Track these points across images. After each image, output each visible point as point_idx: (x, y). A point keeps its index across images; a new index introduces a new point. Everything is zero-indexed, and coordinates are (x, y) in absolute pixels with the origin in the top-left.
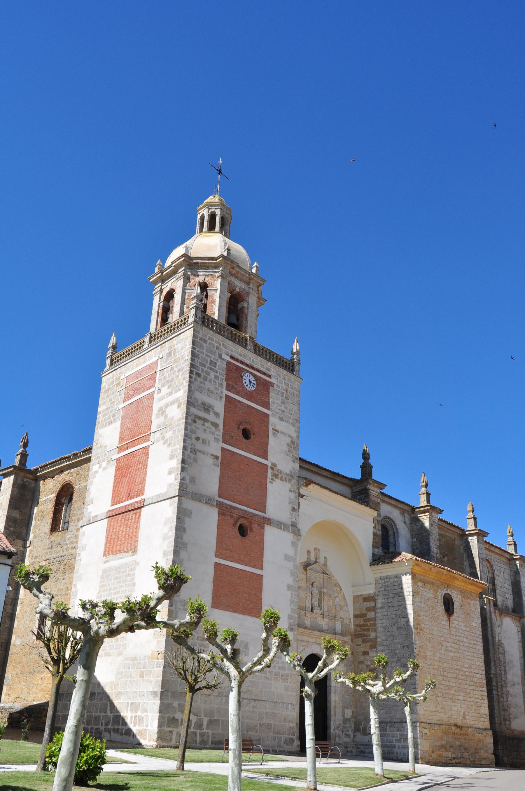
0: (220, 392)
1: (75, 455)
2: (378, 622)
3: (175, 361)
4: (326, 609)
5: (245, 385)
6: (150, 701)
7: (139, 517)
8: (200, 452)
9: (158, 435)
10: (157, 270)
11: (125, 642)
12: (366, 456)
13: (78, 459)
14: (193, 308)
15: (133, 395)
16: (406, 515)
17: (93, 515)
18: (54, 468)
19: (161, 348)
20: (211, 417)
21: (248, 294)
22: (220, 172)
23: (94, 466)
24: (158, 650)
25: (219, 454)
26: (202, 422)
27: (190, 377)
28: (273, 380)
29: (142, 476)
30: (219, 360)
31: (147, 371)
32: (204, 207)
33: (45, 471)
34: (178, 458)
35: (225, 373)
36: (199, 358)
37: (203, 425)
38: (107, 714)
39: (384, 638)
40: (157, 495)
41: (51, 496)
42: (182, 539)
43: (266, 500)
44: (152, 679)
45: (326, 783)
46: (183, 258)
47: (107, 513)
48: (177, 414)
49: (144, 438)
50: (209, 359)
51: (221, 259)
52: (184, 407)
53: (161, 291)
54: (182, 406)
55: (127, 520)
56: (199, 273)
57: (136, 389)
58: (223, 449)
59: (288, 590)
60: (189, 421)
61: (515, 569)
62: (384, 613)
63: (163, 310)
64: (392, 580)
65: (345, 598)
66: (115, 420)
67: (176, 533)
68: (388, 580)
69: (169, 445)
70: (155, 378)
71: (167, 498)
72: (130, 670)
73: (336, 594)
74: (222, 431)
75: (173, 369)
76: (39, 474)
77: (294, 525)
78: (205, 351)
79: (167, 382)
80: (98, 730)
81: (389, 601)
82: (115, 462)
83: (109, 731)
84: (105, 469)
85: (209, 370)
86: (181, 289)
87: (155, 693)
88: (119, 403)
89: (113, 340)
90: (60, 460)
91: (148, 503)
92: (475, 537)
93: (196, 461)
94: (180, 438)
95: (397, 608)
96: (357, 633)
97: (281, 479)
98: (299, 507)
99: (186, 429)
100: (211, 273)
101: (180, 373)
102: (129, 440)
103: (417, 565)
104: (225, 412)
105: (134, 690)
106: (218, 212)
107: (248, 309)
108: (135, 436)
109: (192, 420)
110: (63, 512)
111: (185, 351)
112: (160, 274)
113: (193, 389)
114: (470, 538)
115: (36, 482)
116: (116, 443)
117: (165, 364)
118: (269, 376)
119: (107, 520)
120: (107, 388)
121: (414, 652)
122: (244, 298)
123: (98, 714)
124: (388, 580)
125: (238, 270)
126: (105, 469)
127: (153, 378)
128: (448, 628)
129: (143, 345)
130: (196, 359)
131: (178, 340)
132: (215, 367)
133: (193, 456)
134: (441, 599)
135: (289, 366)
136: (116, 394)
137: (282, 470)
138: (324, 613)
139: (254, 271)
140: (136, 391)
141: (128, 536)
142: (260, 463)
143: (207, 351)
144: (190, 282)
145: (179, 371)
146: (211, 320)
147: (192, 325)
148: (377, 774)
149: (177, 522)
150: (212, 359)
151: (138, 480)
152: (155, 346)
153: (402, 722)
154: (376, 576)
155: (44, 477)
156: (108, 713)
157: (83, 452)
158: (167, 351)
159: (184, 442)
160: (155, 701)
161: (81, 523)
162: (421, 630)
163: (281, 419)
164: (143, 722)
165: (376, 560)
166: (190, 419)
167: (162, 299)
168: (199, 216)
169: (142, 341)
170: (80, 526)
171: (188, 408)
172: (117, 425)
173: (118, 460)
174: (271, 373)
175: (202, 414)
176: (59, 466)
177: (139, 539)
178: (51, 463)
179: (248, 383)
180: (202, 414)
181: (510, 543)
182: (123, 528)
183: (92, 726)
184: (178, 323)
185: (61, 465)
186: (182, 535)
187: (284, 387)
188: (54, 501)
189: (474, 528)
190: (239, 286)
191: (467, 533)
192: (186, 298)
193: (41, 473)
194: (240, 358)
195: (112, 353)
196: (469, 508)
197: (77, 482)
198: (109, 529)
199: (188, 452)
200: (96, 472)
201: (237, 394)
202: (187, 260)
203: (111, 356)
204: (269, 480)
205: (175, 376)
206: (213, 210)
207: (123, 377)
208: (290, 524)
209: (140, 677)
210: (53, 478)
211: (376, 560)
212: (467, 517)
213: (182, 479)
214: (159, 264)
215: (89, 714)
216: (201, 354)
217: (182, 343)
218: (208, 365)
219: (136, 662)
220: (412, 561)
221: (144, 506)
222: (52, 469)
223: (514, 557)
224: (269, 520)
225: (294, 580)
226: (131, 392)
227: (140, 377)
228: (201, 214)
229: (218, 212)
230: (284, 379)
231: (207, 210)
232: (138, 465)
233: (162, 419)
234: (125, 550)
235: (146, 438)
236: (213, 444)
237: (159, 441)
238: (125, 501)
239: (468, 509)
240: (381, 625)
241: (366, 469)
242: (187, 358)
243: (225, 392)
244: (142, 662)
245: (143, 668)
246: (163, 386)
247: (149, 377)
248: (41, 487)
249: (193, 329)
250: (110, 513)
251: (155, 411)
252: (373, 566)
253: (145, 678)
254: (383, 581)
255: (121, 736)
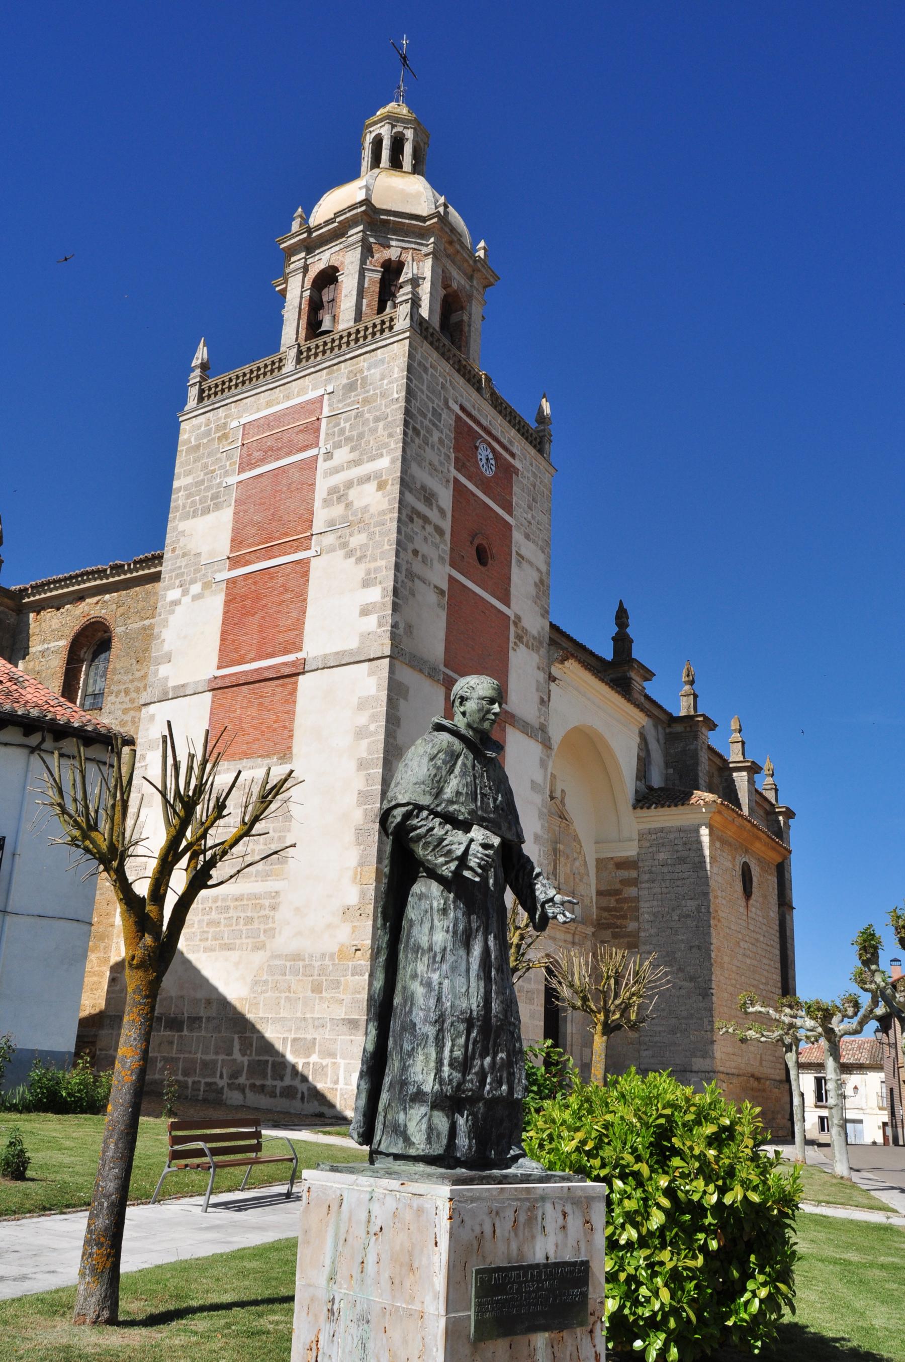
0: (446, 471)
1: (118, 569)
2: (642, 904)
3: (366, 401)
4: (562, 881)
5: (481, 464)
6: (342, 1037)
7: (295, 690)
8: (419, 578)
9: (329, 539)
10: (295, 226)
11: (271, 925)
12: (622, 617)
13: (123, 577)
14: (406, 301)
15: (263, 461)
16: (660, 728)
17: (171, 684)
18: (66, 590)
19: (328, 374)
20: (433, 515)
21: (470, 297)
22: (405, 61)
23: (169, 591)
24: (355, 942)
25: (445, 586)
26: (421, 522)
27: (405, 433)
28: (517, 464)
29: (294, 615)
30: (445, 410)
31: (296, 416)
32: (381, 120)
33: (43, 596)
34: (384, 585)
35: (453, 436)
36: (416, 400)
37: (424, 528)
38: (234, 1057)
39: (653, 931)
40: (337, 653)
41: (57, 643)
42: (395, 738)
43: (507, 681)
44: (342, 996)
45: (828, 1203)
46: (363, 208)
47: (210, 681)
48: (379, 501)
49: (295, 544)
50: (431, 405)
51: (435, 220)
52: (394, 489)
53: (306, 269)
54: (389, 487)
55: (261, 697)
56: (393, 243)
57: (271, 449)
58: (451, 579)
59: (535, 843)
60: (404, 517)
61: (776, 829)
62: (655, 891)
63: (310, 305)
64: (671, 836)
65: (585, 862)
66: (217, 507)
67: (386, 727)
68: (662, 835)
69: (359, 560)
70: (318, 430)
71: (363, 659)
72: (287, 977)
73: (575, 855)
74: (449, 545)
75: (362, 416)
76: (26, 600)
77: (543, 728)
78: (425, 388)
79: (349, 439)
80: (214, 1087)
81: (665, 870)
82: (224, 585)
83: (241, 1089)
84: (196, 598)
85: (431, 426)
86: (358, 268)
87: (352, 1024)
88: (227, 474)
89: (202, 353)
90: (82, 575)
91: (314, 667)
92: (745, 773)
93: (414, 595)
94: (386, 547)
95: (679, 883)
96: (603, 921)
97: (527, 646)
98: (549, 697)
99: (399, 531)
100: (413, 246)
101: (381, 425)
102: (258, 545)
103: (719, 812)
104: (453, 511)
105: (299, 1015)
106: (409, 134)
107: (469, 326)
108: (271, 539)
109: (407, 515)
110: (83, 676)
111: (390, 383)
112: (305, 235)
113: (408, 457)
114: (735, 774)
115: (18, 615)
116: (223, 547)
117: (340, 405)
118: (513, 455)
119: (210, 694)
120: (193, 443)
121: (710, 958)
122: (464, 304)
123: (211, 1057)
124: (662, 835)
125: (458, 247)
126: (196, 598)
127: (313, 429)
128: (745, 917)
129: (280, 368)
130: (414, 401)
131: (372, 360)
132: (440, 422)
133: (409, 584)
134: (738, 869)
135: (538, 440)
136: (219, 455)
137: (529, 629)
138: (561, 887)
139: (481, 253)
140: (270, 453)
141: (267, 728)
142: (499, 611)
143: (428, 387)
144: (373, 257)
145: (377, 420)
146: (431, 330)
147: (408, 334)
148: (842, 1178)
149: (387, 707)
150: (435, 405)
151: (285, 622)
152: (312, 370)
153: (685, 1071)
154: (641, 827)
155: (39, 607)
156: (237, 1055)
157: (135, 563)
158: (345, 381)
159: (397, 555)
160: (353, 1037)
161: (145, 697)
162: (719, 920)
163: (527, 537)
164: (326, 1075)
165: (646, 798)
166: (404, 513)
167: (308, 285)
168: (369, 138)
169: (276, 359)
170: (142, 702)
171: (401, 493)
172: (225, 518)
173: (231, 582)
174: (515, 450)
175: (421, 507)
176: (76, 587)
177: (296, 733)
178: (60, 581)
179: (484, 461)
180: (421, 507)
181: (769, 787)
182: (252, 711)
183: (196, 1079)
184: (349, 334)
185: (82, 586)
186: (395, 731)
187: (532, 479)
188: (65, 654)
189: (742, 759)
190: (458, 280)
191: (731, 765)
192: (366, 286)
193: (32, 599)
194: (474, 413)
195: (201, 376)
196: (734, 725)
197: (120, 621)
198: (215, 711)
199: (402, 577)
200: (176, 603)
201: (470, 478)
202: (370, 212)
203: (200, 382)
204: (511, 645)
205: (366, 429)
206: (399, 129)
207: (234, 424)
208: (538, 727)
209: (313, 991)
210: (58, 609)
211: (646, 798)
212: (730, 740)
213: (394, 626)
214: (301, 216)
215: (220, 1062)
216: (419, 393)
217: (386, 366)
218: (430, 415)
219: (301, 963)
220: (714, 805)
221: (303, 673)
222: (60, 591)
223: (777, 810)
224: (513, 716)
225: (543, 826)
226: (257, 454)
227: (278, 427)
228: (373, 135)
229: (409, 134)
230: (531, 465)
231: (387, 127)
232: (282, 593)
233: (338, 510)
234: (261, 752)
235: (304, 543)
236: (437, 565)
237: (334, 550)
238: (254, 660)
239: (733, 728)
240: (649, 910)
241: (622, 642)
242: (396, 396)
243: (454, 472)
244: (317, 964)
245: (319, 975)
246: (337, 445)
247: (301, 427)
248: (31, 626)
249: (407, 341)
250: (217, 681)
251: (321, 491)
252: (645, 812)
253: (324, 994)
254: (654, 836)
255: (272, 1100)
